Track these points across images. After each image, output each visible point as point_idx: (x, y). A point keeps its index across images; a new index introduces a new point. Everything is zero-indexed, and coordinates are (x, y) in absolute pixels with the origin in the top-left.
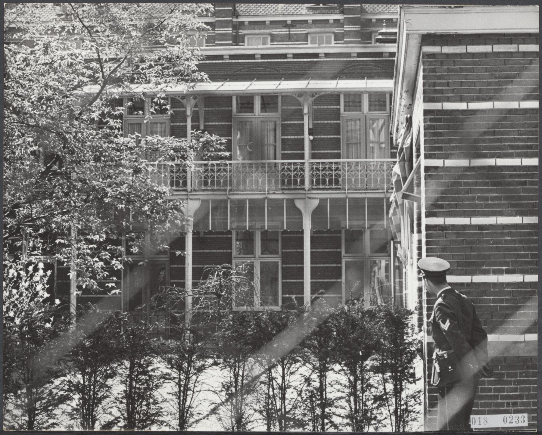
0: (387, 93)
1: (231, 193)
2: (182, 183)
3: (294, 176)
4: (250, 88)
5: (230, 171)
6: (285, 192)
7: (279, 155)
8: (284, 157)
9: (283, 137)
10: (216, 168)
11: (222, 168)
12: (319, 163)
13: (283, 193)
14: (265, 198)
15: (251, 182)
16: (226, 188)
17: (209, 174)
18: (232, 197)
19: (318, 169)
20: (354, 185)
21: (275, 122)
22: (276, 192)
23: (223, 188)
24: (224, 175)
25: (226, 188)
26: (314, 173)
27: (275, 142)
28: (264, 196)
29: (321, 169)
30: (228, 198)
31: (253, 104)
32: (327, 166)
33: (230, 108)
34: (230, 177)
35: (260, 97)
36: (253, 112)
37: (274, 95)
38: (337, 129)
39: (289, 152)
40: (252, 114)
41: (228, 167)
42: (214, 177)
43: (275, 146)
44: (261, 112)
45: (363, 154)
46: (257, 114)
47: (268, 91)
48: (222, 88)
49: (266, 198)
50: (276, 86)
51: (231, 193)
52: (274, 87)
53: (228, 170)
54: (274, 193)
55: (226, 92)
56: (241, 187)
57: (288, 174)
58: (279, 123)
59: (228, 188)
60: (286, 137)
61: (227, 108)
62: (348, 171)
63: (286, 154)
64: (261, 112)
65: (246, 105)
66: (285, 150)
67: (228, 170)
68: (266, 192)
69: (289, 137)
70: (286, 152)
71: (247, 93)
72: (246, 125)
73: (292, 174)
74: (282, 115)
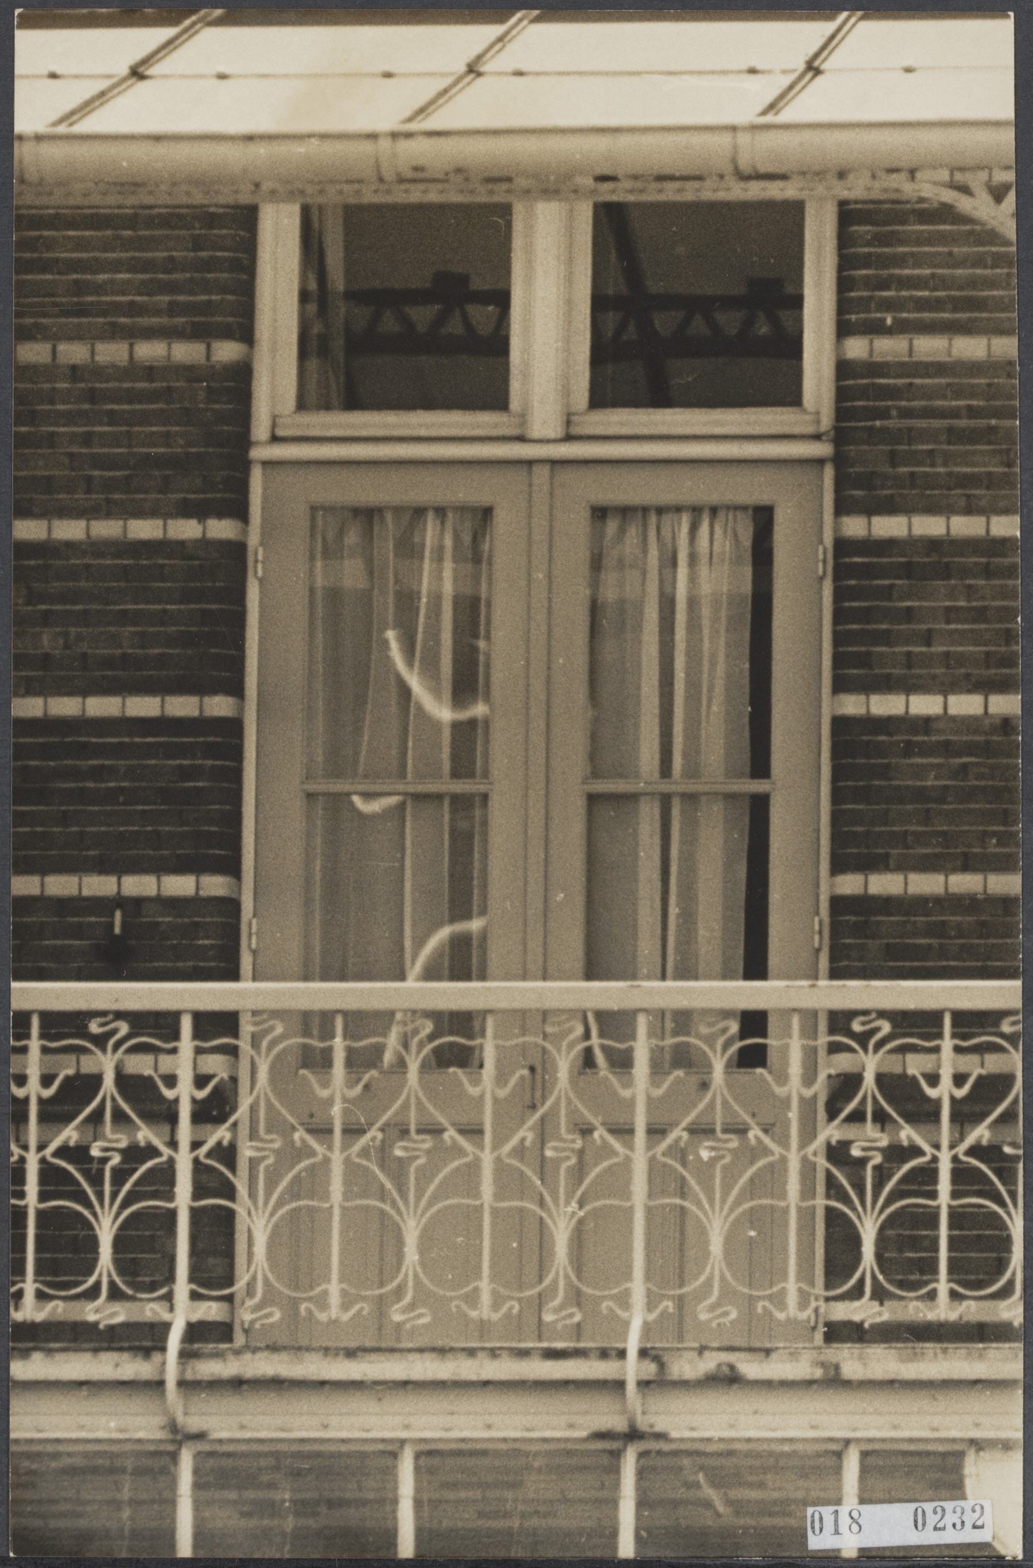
0: (552, 185)
1: (208, 1369)
2: (119, 1243)
3: (961, 1175)
4: (468, 110)
5: (214, 1108)
6: (853, 1363)
7: (795, 917)
8: (860, 940)
9: (852, 705)
10: (948, 1062)
11: (105, 1064)
12: (919, 1025)
13: (833, 1381)
14: (613, 1442)
15: (451, 1247)
16: (151, 1310)
17: (109, 1144)
18: (226, 1422)
19: (906, 1098)
20: (577, 1298)
21: (763, 518)
22: (751, 1368)
23: (119, 1314)
24: (135, 1154)
25: (151, 1310)
26: (868, 1140)
27: (760, 767)
28: (604, 1415)
29: (944, 1091)
30: (180, 1436)
31: (502, 299)
32: (105, 1064)
33: (227, 351)
34: (212, 1181)
35: (295, 209)
36: (496, 398)
37: (738, 192)
38: (198, 620)
39: (926, 884)
40: (485, 421)
41: (184, 1059)
42: (928, 1174)
43: (759, 809)
44: (598, 400)
45: (714, 923)
46: (544, 421)
47: (664, 153)
48: (132, 113)
49: (633, 1435)
50: (766, 89)
51: (208, 1369)
52: (741, 103)
53: (185, 1094)
54: (729, 1379)
55: (183, 152)
56: (334, 1301)
57: (898, 1153)
58: (808, 535)
59: (182, 1310)
60: (886, 705)
61: (186, 352)
62: (656, 1132)
63: (886, 904)
64: (598, 400)
65: (422, 315)
66: (868, 865)
67: (185, 1094)
68: (632, 1369)
69: (924, 705)
70: (884, 884)
71: (418, 175)
72: (409, 549)
73: (944, 1150)
74: (840, 436)
